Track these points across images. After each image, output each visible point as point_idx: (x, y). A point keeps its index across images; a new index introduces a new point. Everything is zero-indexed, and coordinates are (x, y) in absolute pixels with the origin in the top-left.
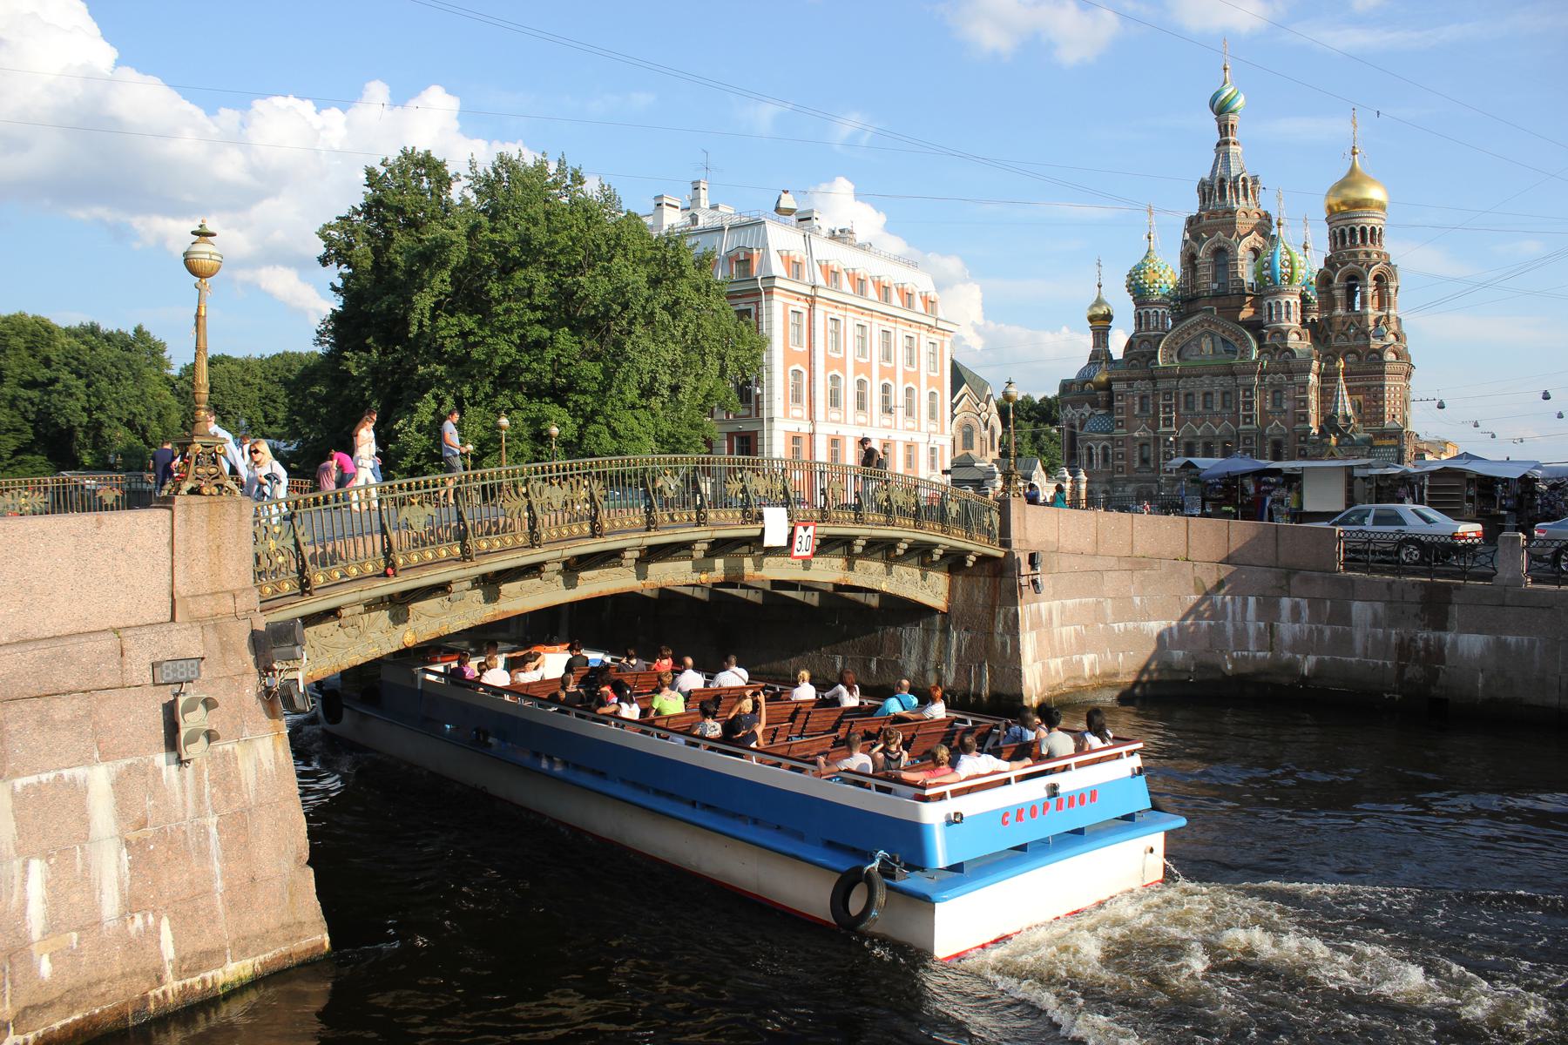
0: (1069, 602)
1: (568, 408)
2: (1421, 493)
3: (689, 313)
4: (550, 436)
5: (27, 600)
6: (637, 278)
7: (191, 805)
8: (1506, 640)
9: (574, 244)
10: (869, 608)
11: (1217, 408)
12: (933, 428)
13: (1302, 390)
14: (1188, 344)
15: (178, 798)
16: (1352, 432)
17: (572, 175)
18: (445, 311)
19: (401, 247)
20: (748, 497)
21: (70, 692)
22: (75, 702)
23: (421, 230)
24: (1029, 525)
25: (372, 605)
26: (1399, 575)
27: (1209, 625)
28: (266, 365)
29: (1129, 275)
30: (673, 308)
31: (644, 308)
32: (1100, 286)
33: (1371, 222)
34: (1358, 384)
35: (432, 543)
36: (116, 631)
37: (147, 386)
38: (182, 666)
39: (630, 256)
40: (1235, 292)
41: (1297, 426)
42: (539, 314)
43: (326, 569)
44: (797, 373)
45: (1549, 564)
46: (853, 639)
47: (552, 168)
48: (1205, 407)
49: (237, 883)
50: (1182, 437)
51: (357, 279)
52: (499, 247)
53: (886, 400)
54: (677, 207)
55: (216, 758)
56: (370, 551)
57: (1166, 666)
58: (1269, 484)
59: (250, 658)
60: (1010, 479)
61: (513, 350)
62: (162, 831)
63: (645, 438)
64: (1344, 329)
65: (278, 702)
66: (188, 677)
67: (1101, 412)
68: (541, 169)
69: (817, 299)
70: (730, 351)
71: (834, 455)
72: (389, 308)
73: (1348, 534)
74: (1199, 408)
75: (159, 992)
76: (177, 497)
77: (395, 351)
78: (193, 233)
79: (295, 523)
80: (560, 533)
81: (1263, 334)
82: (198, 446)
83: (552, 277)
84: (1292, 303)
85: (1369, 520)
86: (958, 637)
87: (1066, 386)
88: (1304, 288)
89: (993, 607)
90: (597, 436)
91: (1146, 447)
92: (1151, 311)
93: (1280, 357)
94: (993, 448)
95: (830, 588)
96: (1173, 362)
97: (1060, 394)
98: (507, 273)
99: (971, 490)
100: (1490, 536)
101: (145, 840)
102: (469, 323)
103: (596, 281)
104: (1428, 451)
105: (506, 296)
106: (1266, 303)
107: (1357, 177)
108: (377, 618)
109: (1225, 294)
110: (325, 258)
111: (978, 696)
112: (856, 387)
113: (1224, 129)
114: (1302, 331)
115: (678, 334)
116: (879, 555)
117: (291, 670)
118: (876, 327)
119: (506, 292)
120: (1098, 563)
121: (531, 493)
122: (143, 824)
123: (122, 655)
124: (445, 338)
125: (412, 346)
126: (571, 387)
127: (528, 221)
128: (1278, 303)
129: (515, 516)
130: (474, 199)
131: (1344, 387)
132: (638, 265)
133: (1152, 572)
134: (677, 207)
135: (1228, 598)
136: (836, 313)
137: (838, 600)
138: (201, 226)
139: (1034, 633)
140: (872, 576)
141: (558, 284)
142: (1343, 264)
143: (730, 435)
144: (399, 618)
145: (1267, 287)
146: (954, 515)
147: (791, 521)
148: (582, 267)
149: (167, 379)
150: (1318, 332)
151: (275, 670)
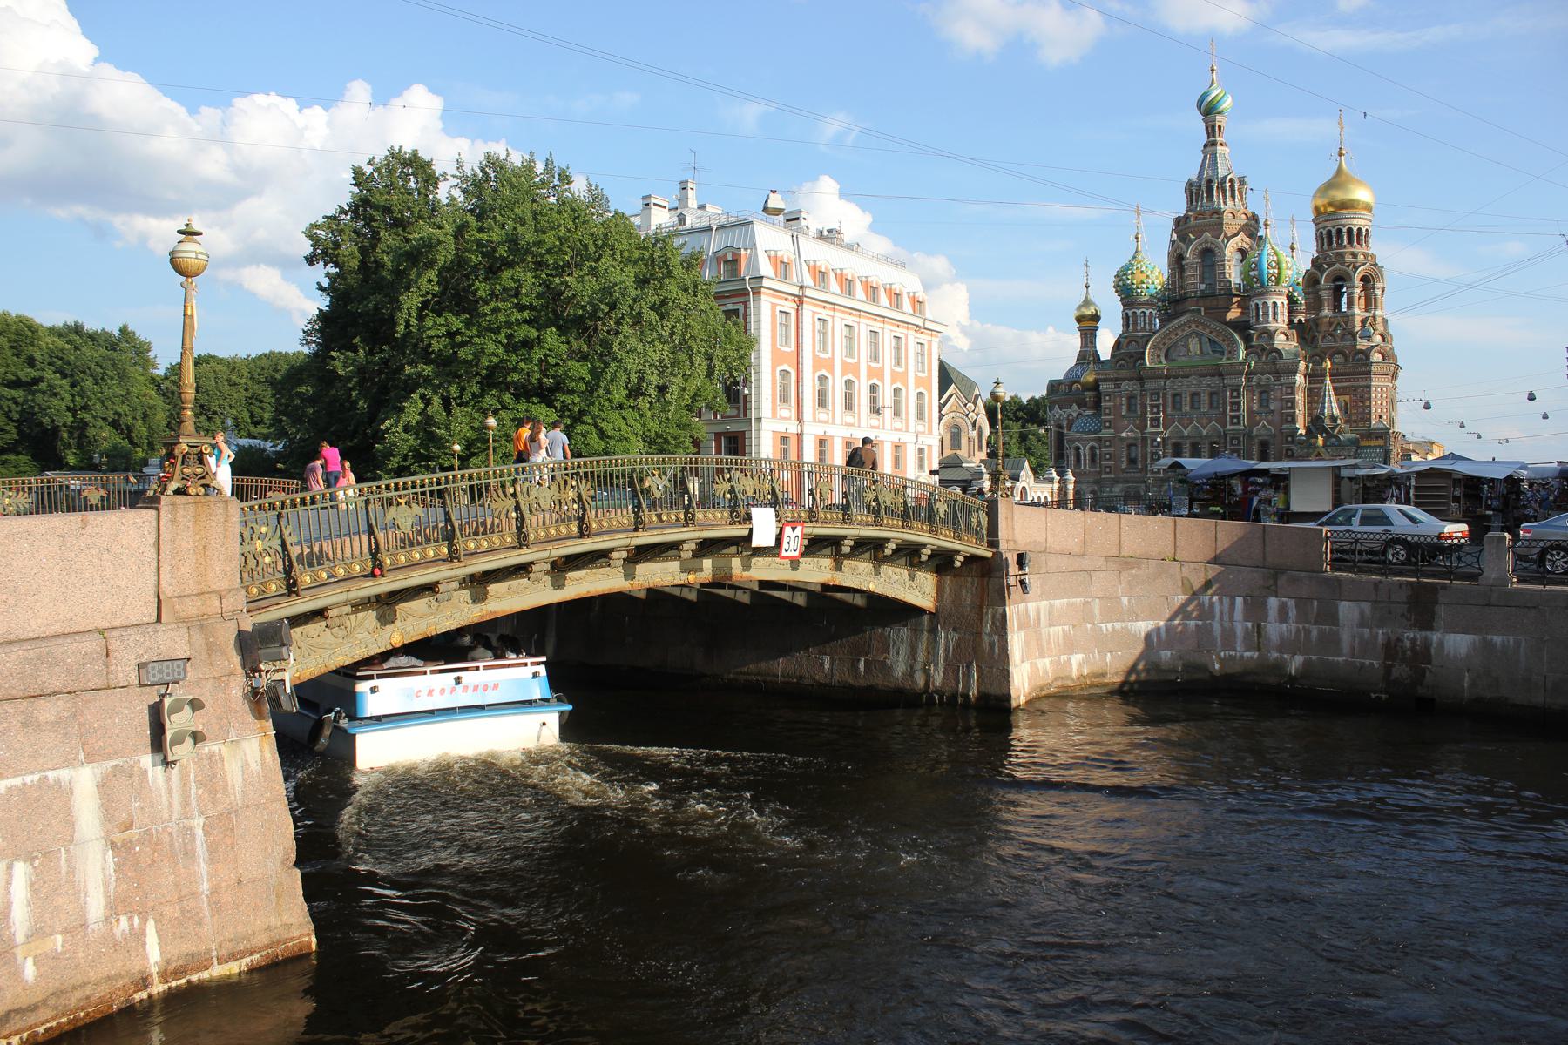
0: (1057, 603)
1: (555, 408)
2: (1408, 493)
5: (11, 601)
6: (624, 278)
9: (561, 244)
10: (856, 608)
11: (1204, 409)
12: (920, 428)
13: (1289, 391)
14: (1175, 344)
15: (164, 799)
16: (1339, 432)
19: (388, 247)
20: (736, 497)
21: (55, 693)
22: (60, 703)
23: (408, 229)
24: (1017, 525)
25: (359, 606)
26: (1385, 574)
27: (1197, 626)
28: (252, 365)
29: (1117, 276)
30: (660, 308)
31: (632, 308)
32: (1087, 287)
33: (1357, 223)
36: (101, 631)
38: (168, 667)
39: (618, 256)
40: (1222, 293)
41: (1284, 426)
42: (526, 314)
44: (785, 373)
45: (1535, 564)
47: (540, 168)
48: (1192, 407)
49: (224, 884)
51: (344, 279)
53: (873, 400)
54: (665, 207)
55: (202, 759)
57: (1154, 666)
58: (1257, 484)
59: (236, 659)
60: (998, 479)
61: (501, 350)
62: (148, 833)
63: (633, 438)
67: (1089, 412)
68: (528, 168)
69: (805, 299)
71: (822, 454)
72: (376, 308)
73: (1335, 535)
74: (1186, 408)
76: (163, 497)
77: (382, 351)
81: (1250, 335)
82: (184, 446)
83: (539, 277)
85: (1356, 521)
86: (946, 637)
87: (1053, 387)
88: (1291, 289)
89: (981, 608)
90: (584, 436)
91: (1134, 448)
92: (1139, 312)
94: (980, 448)
95: (818, 589)
96: (1161, 362)
97: (1048, 395)
98: (495, 273)
99: (959, 491)
100: (1476, 535)
101: (131, 841)
102: (457, 323)
103: (583, 281)
104: (1414, 451)
105: (493, 295)
107: (1343, 178)
108: (364, 619)
110: (312, 257)
111: (966, 696)
113: (1211, 130)
114: (1289, 332)
115: (666, 334)
116: (867, 555)
118: (864, 327)
120: (1086, 563)
123: (107, 655)
124: (432, 337)
125: (399, 345)
126: (558, 387)
127: (515, 220)
129: (503, 516)
130: (461, 199)
131: (1331, 388)
132: (625, 265)
134: (665, 207)
136: (825, 314)
137: (826, 599)
138: (187, 225)
139: (1022, 633)
140: (860, 576)
141: (546, 284)
142: (1330, 265)
143: (718, 435)
144: (386, 619)
145: (1254, 288)
147: (779, 521)
148: (569, 267)
149: (153, 379)
150: (1305, 332)
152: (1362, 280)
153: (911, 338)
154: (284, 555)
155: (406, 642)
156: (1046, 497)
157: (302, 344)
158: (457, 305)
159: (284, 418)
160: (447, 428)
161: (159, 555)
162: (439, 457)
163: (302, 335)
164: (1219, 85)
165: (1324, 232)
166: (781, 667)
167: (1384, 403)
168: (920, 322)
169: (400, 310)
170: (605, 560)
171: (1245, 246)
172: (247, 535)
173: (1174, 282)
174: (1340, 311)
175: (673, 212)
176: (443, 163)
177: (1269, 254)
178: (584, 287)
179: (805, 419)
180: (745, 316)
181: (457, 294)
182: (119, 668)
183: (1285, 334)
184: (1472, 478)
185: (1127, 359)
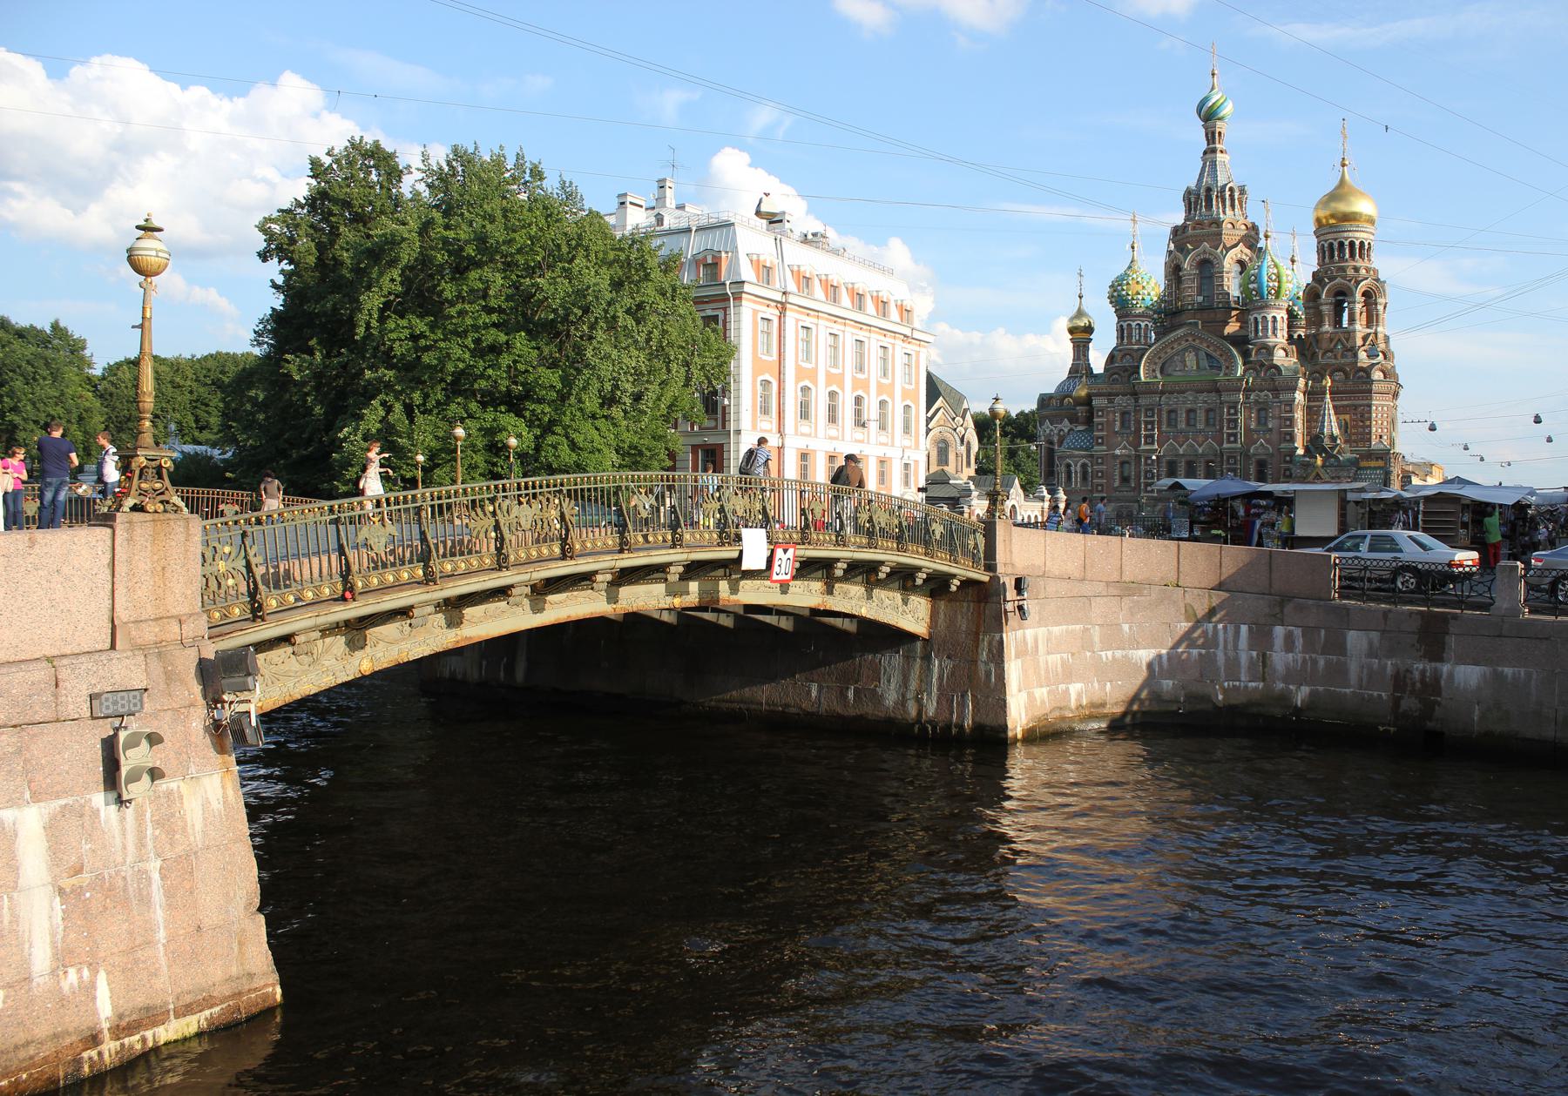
0: (1056, 630)
1: (524, 417)
2: (1415, 518)
3: (654, 318)
4: (506, 447)
6: (599, 280)
7: (131, 848)
8: (1503, 671)
9: (533, 243)
10: (845, 633)
11: (1201, 426)
12: (907, 443)
13: (1288, 408)
15: (118, 841)
16: (1339, 452)
17: (531, 170)
18: (394, 312)
19: (347, 243)
20: (725, 517)
23: (369, 225)
24: (1015, 549)
25: (328, 631)
26: (1395, 603)
27: (1200, 654)
28: (197, 366)
30: (637, 312)
31: (606, 311)
32: (1081, 297)
33: (1359, 236)
34: (1346, 403)
35: (393, 565)
36: (50, 659)
37: (67, 387)
38: (123, 698)
39: (593, 257)
40: (1220, 306)
41: (1283, 446)
42: (495, 317)
43: (279, 592)
44: (766, 383)
45: (1547, 593)
46: (830, 666)
47: (510, 164)
48: (1188, 424)
49: (182, 932)
50: (1164, 456)
51: (300, 276)
52: (451, 244)
53: (858, 413)
54: (641, 206)
55: (159, 797)
56: (325, 571)
57: (1156, 696)
58: (1259, 506)
59: (197, 689)
60: (997, 500)
61: (467, 356)
62: (100, 877)
63: (606, 450)
64: (1332, 345)
65: (227, 736)
66: (129, 710)
67: (1081, 428)
68: (498, 163)
69: (788, 306)
70: (696, 359)
71: (804, 470)
72: (335, 309)
73: (1344, 561)
74: (1181, 425)
75: (93, 1053)
76: (118, 514)
77: (340, 354)
78: (138, 227)
79: (247, 543)
80: (540, 552)
81: (1248, 350)
82: (142, 459)
83: (509, 278)
84: (1279, 319)
85: (1364, 547)
86: (940, 665)
87: (1044, 400)
88: (1291, 303)
89: (977, 634)
90: (555, 447)
91: (1127, 465)
92: (1134, 324)
93: (1265, 374)
94: (968, 464)
95: (807, 613)
96: (1156, 377)
97: (1038, 409)
98: (461, 274)
99: (945, 509)
100: (1488, 561)
101: (81, 887)
102: (421, 326)
103: (555, 283)
104: (1413, 473)
105: (460, 297)
106: (1252, 318)
107: (1346, 190)
108: (331, 645)
109: (1210, 308)
110: (265, 253)
111: (961, 727)
112: (828, 399)
113: (1211, 136)
114: (1289, 348)
115: (641, 339)
116: (859, 578)
117: (242, 702)
118: (849, 335)
119: (460, 293)
120: (1087, 589)
121: (498, 511)
122: (78, 871)
123: (57, 686)
124: (394, 340)
125: (358, 348)
126: (527, 395)
127: (484, 218)
128: (1265, 318)
129: (482, 535)
130: (427, 194)
131: (1331, 406)
132: (600, 267)
133: (1143, 598)
134: (641, 206)
135: (1220, 626)
136: (808, 322)
137: (812, 623)
138: (147, 220)
139: (1019, 661)
140: (852, 600)
141: (516, 286)
142: (1332, 279)
143: (695, 448)
144: (355, 644)
145: (1254, 301)
146: (938, 538)
147: (770, 543)
148: (540, 268)
149: (89, 379)
150: (1304, 348)
151: (225, 702)
152: (1363, 295)
153: (898, 349)
154: (249, 578)
155: (376, 669)
156: (1036, 517)
157: (253, 346)
158: (420, 306)
159: (234, 424)
160: (410, 437)
161: (113, 576)
162: (401, 468)
163: (253, 336)
164: (1220, 90)
165: (1326, 245)
166: (765, 695)
167: (1385, 423)
168: (907, 332)
169: (360, 310)
170: (588, 582)
171: (1244, 257)
172: (209, 555)
173: (1170, 294)
174: (1341, 326)
175: (650, 212)
176: (408, 156)
177: (1268, 267)
178: (556, 289)
179: (786, 432)
180: (725, 322)
181: (420, 294)
182: (70, 699)
183: (1284, 350)
184: (1481, 503)
185: (1121, 372)
